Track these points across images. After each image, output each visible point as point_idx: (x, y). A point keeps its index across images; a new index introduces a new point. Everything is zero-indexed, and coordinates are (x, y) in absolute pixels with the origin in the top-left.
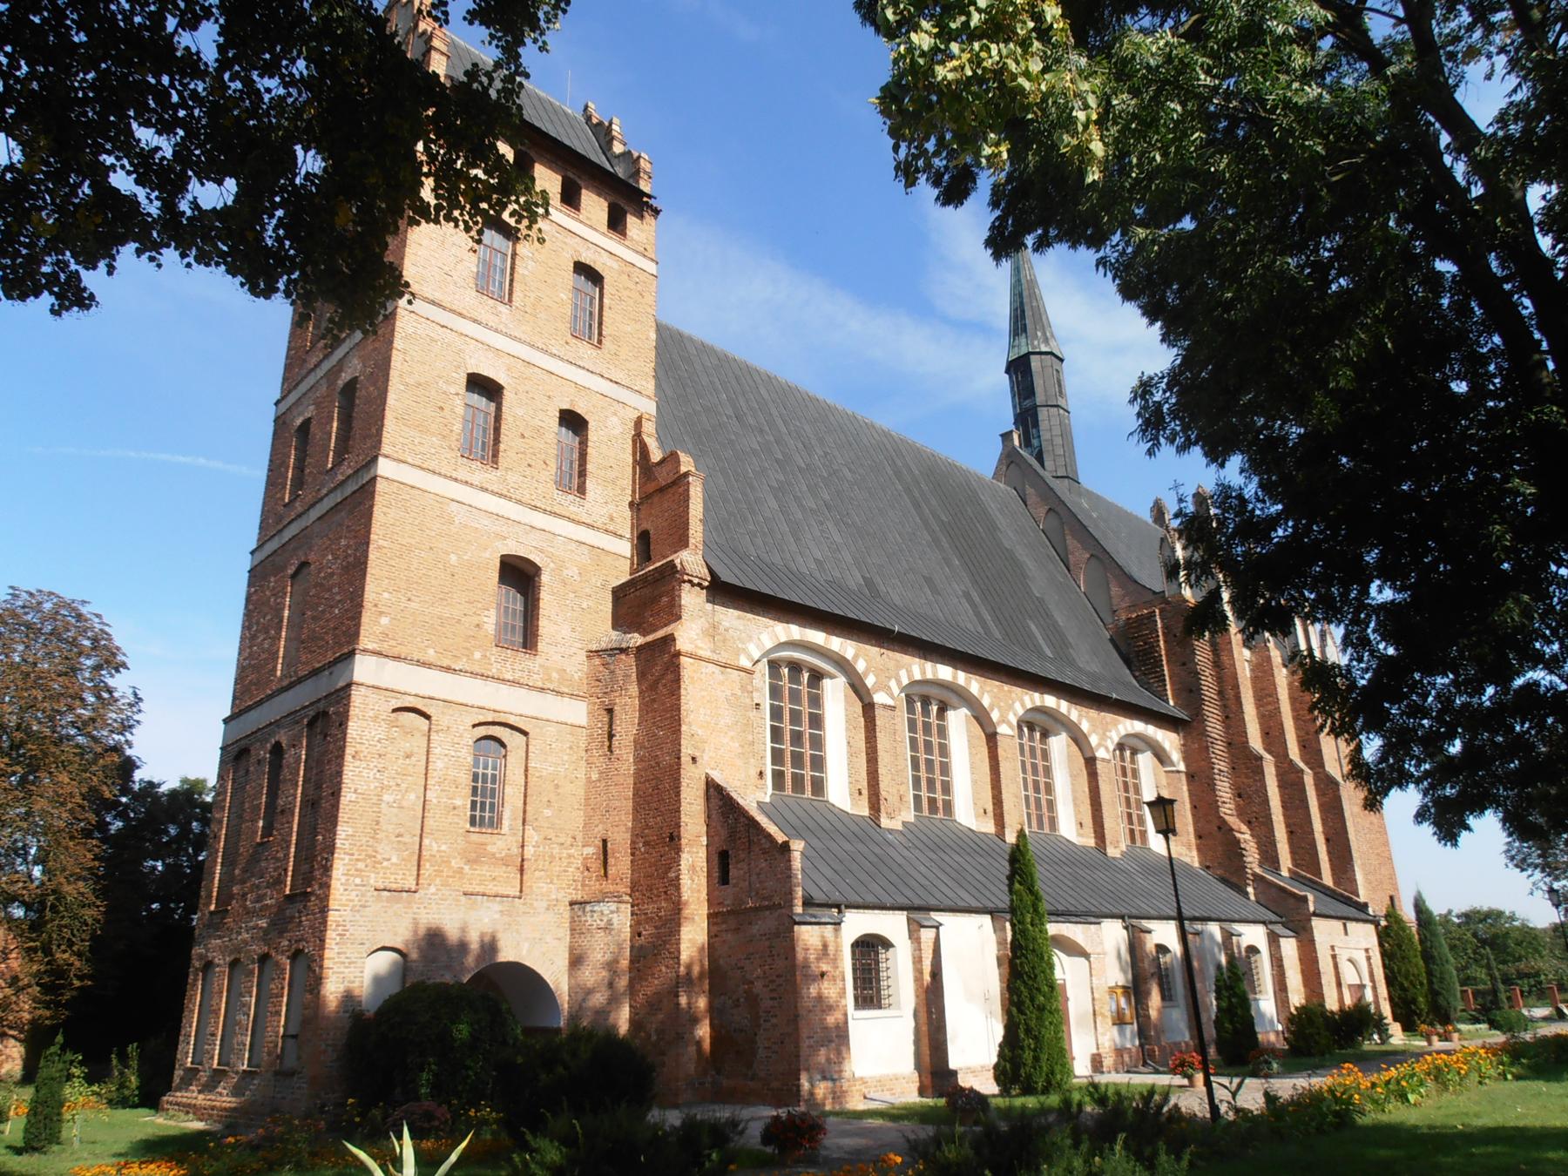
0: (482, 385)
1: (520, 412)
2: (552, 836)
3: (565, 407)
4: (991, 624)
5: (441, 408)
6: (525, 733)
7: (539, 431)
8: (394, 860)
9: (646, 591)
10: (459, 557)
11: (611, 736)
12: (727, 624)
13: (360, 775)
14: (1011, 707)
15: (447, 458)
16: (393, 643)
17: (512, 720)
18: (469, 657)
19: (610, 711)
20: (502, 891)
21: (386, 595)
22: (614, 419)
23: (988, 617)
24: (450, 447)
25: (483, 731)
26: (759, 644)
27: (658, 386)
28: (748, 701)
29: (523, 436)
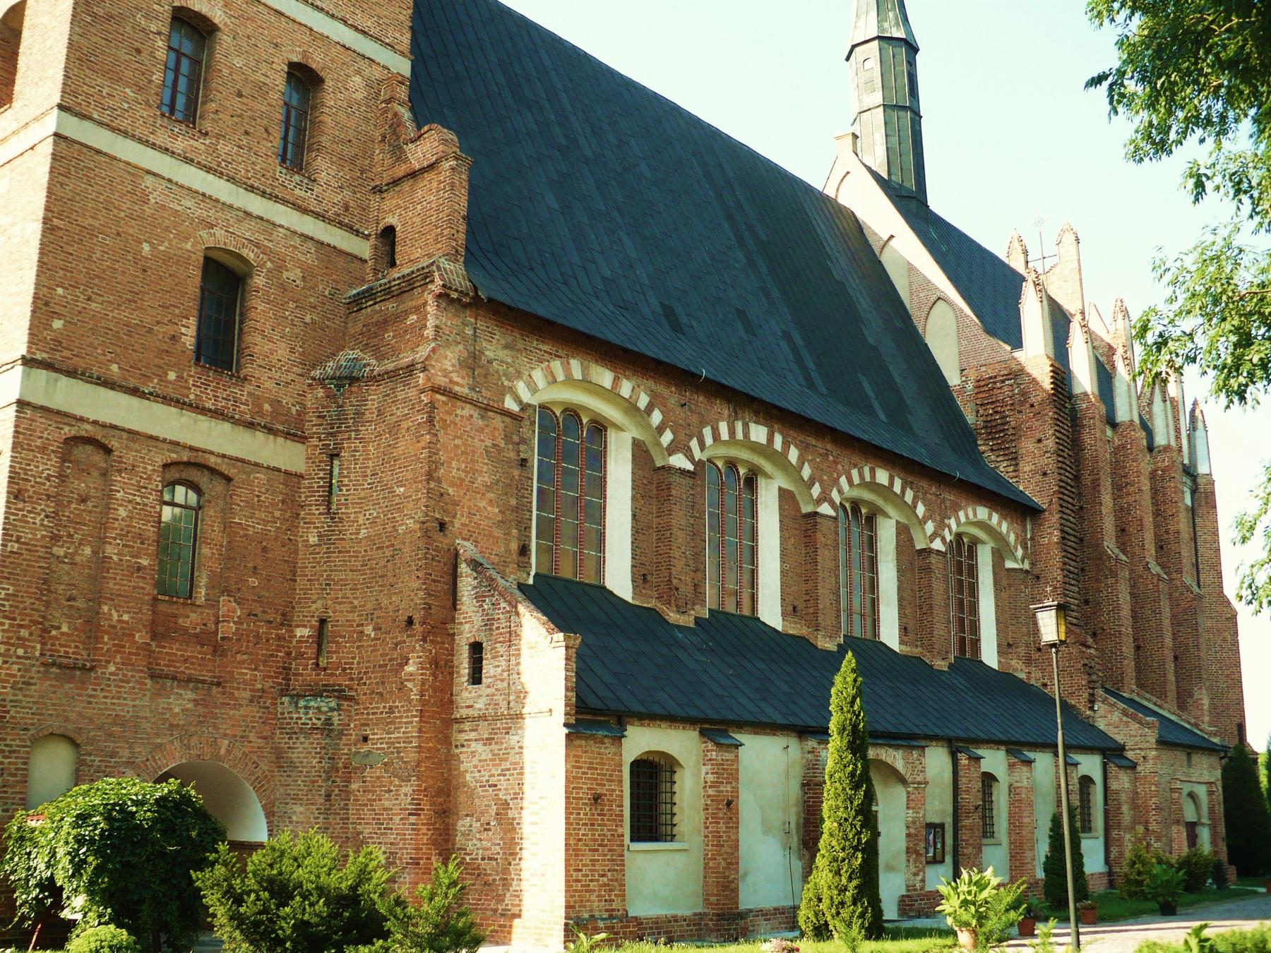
1: (238, 62)
2: (258, 610)
3: (296, 59)
4: (814, 374)
5: (138, 51)
6: (229, 479)
7: (261, 89)
8: (65, 629)
12: (489, 354)
14: (836, 482)
15: (143, 115)
16: (66, 353)
17: (212, 461)
18: (162, 377)
21: (60, 291)
22: (357, 79)
23: (811, 365)
24: (147, 103)
25: (174, 474)
27: (414, 40)
28: (512, 455)
29: (240, 95)
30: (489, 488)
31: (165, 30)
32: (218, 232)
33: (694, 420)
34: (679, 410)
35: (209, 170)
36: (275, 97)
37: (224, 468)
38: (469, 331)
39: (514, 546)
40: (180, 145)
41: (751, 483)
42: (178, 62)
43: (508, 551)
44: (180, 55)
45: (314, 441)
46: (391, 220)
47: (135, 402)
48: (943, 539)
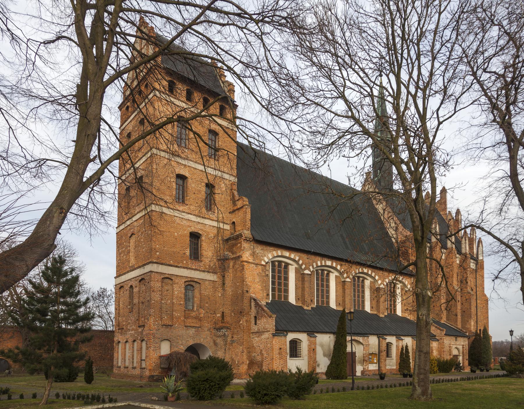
0: (181, 177)
1: (193, 185)
7: (200, 191)
9: (233, 242)
10: (178, 233)
11: (224, 284)
12: (258, 252)
13: (155, 296)
17: (196, 280)
18: (183, 263)
19: (224, 277)
20: (195, 325)
26: (268, 258)
29: (194, 193)
30: (258, 282)
31: (175, 181)
32: (192, 228)
33: (311, 261)
34: (307, 260)
35: (189, 213)
36: (203, 193)
37: (198, 281)
38: (252, 247)
39: (265, 294)
40: (181, 208)
41: (328, 275)
42: (179, 188)
43: (263, 296)
44: (179, 185)
45: (219, 274)
46: (234, 220)
47: (177, 269)
48: (384, 284)
